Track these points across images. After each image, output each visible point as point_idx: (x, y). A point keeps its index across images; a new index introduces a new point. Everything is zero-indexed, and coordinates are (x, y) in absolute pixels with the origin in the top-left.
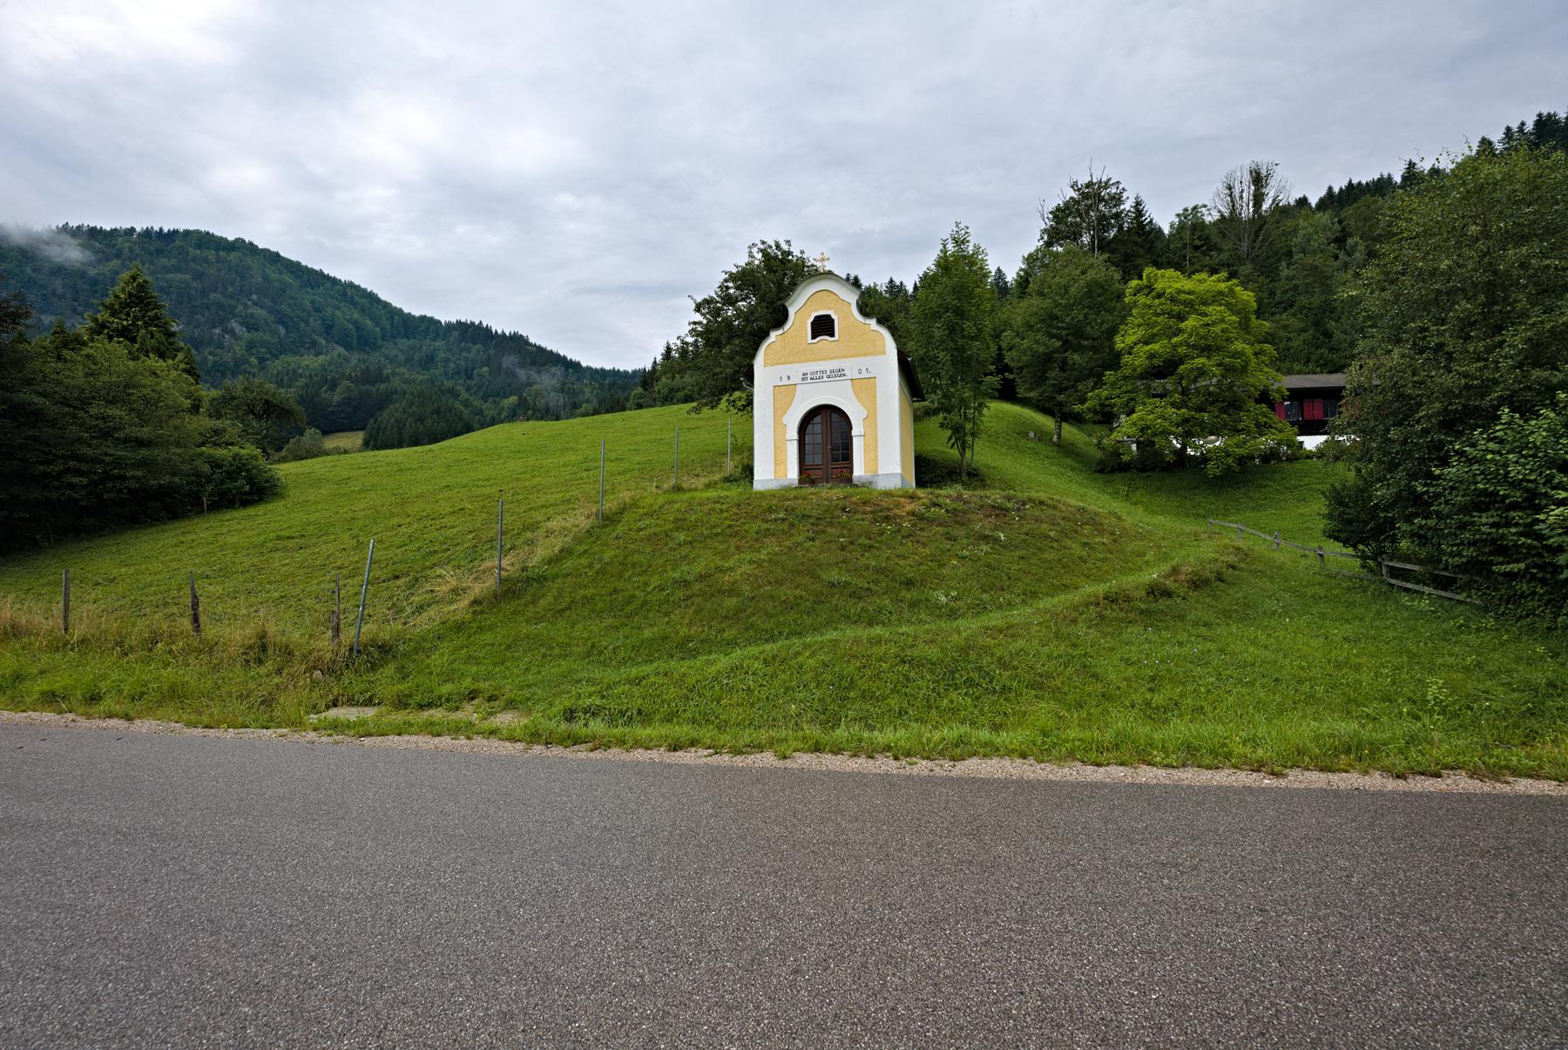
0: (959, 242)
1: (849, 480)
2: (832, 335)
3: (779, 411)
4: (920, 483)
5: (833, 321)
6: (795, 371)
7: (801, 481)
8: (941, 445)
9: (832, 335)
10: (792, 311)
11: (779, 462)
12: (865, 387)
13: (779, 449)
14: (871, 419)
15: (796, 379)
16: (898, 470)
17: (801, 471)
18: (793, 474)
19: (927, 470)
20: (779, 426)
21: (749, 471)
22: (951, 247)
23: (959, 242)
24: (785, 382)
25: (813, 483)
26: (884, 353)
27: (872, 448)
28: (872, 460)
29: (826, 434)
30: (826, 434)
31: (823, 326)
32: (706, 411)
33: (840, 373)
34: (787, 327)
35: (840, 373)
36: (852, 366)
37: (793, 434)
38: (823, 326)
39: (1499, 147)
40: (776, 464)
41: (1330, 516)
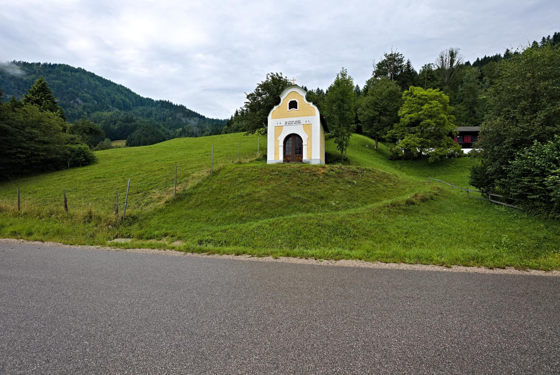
1: (301, 161)
2: (296, 108)
3: (277, 135)
4: (327, 162)
6: (283, 121)
7: (284, 161)
8: (335, 149)
9: (296, 108)
10: (282, 99)
11: (276, 154)
12: (308, 127)
13: (276, 149)
14: (310, 139)
15: (283, 124)
16: (319, 158)
18: (281, 158)
20: (276, 141)
25: (288, 161)
28: (310, 154)
29: (293, 144)
30: (293, 144)
33: (299, 122)
34: (280, 105)
35: (299, 122)
36: (303, 120)
37: (281, 144)
38: (293, 105)
40: (275, 154)
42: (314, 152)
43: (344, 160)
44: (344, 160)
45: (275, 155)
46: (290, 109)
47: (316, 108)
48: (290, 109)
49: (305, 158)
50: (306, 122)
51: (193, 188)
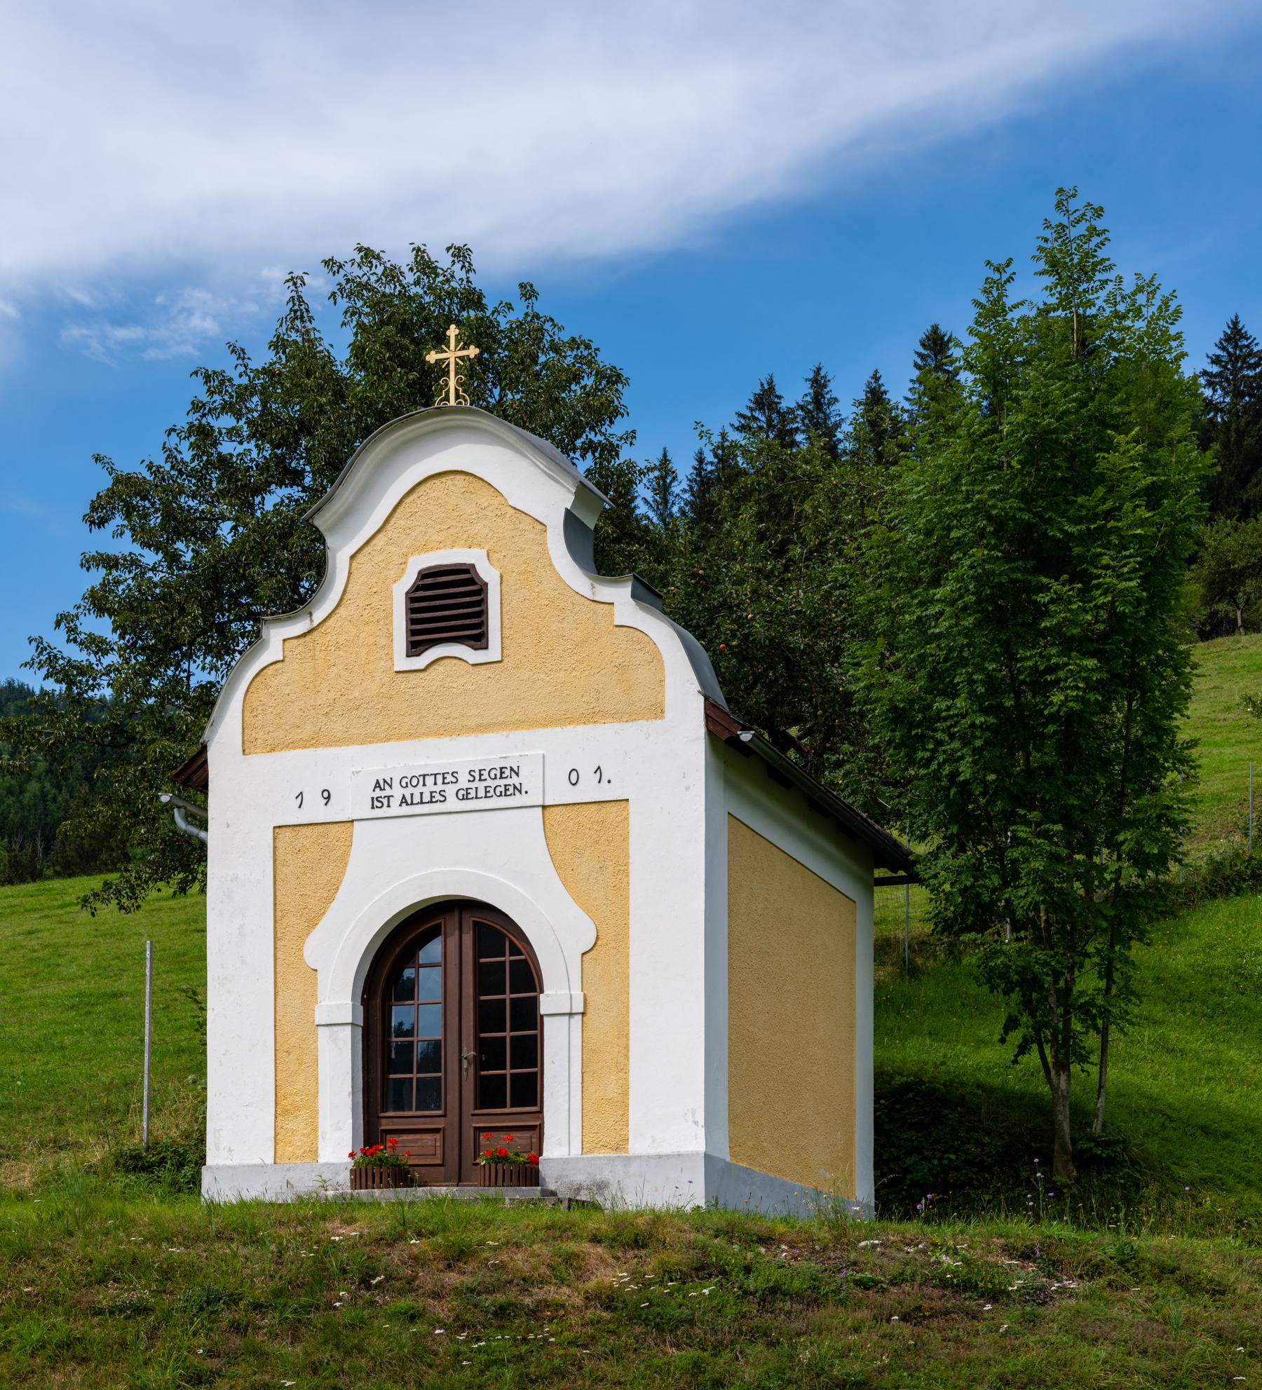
0: (1072, 266)
1: (529, 1174)
2: (478, 639)
3: (294, 915)
4: (895, 1195)
5: (482, 589)
6: (345, 773)
7: (361, 1177)
8: (983, 1053)
9: (478, 639)
10: (340, 555)
11: (291, 1105)
12: (589, 834)
13: (291, 1054)
14: (607, 951)
15: (352, 801)
16: (698, 1144)
17: (372, 1132)
18: (336, 1141)
19: (933, 1145)
20: (290, 975)
21: (314, 1153)
22: (1031, 292)
23: (1072, 266)
24: (315, 811)
25: (401, 1176)
26: (657, 711)
27: (608, 1061)
28: (609, 1112)
29: (455, 1014)
30: (455, 1014)
31: (448, 608)
32: (108, 912)
33: (502, 783)
34: (409, 580)
35: (502, 783)
36: (549, 757)
37: (337, 999)
38: (448, 608)
39: (615, 463)
40: (276, 1113)
41: (668, 1209)
42: (645, 1102)
43: (1084, 1161)
44: (1084, 1161)
45: (281, 1111)
46: (415, 648)
47: (664, 636)
48: (415, 648)
49: (563, 1143)
50: (574, 778)
51: (378, 1241)
